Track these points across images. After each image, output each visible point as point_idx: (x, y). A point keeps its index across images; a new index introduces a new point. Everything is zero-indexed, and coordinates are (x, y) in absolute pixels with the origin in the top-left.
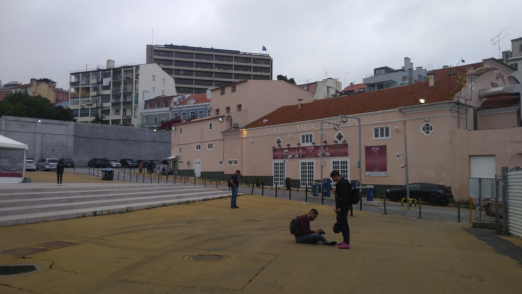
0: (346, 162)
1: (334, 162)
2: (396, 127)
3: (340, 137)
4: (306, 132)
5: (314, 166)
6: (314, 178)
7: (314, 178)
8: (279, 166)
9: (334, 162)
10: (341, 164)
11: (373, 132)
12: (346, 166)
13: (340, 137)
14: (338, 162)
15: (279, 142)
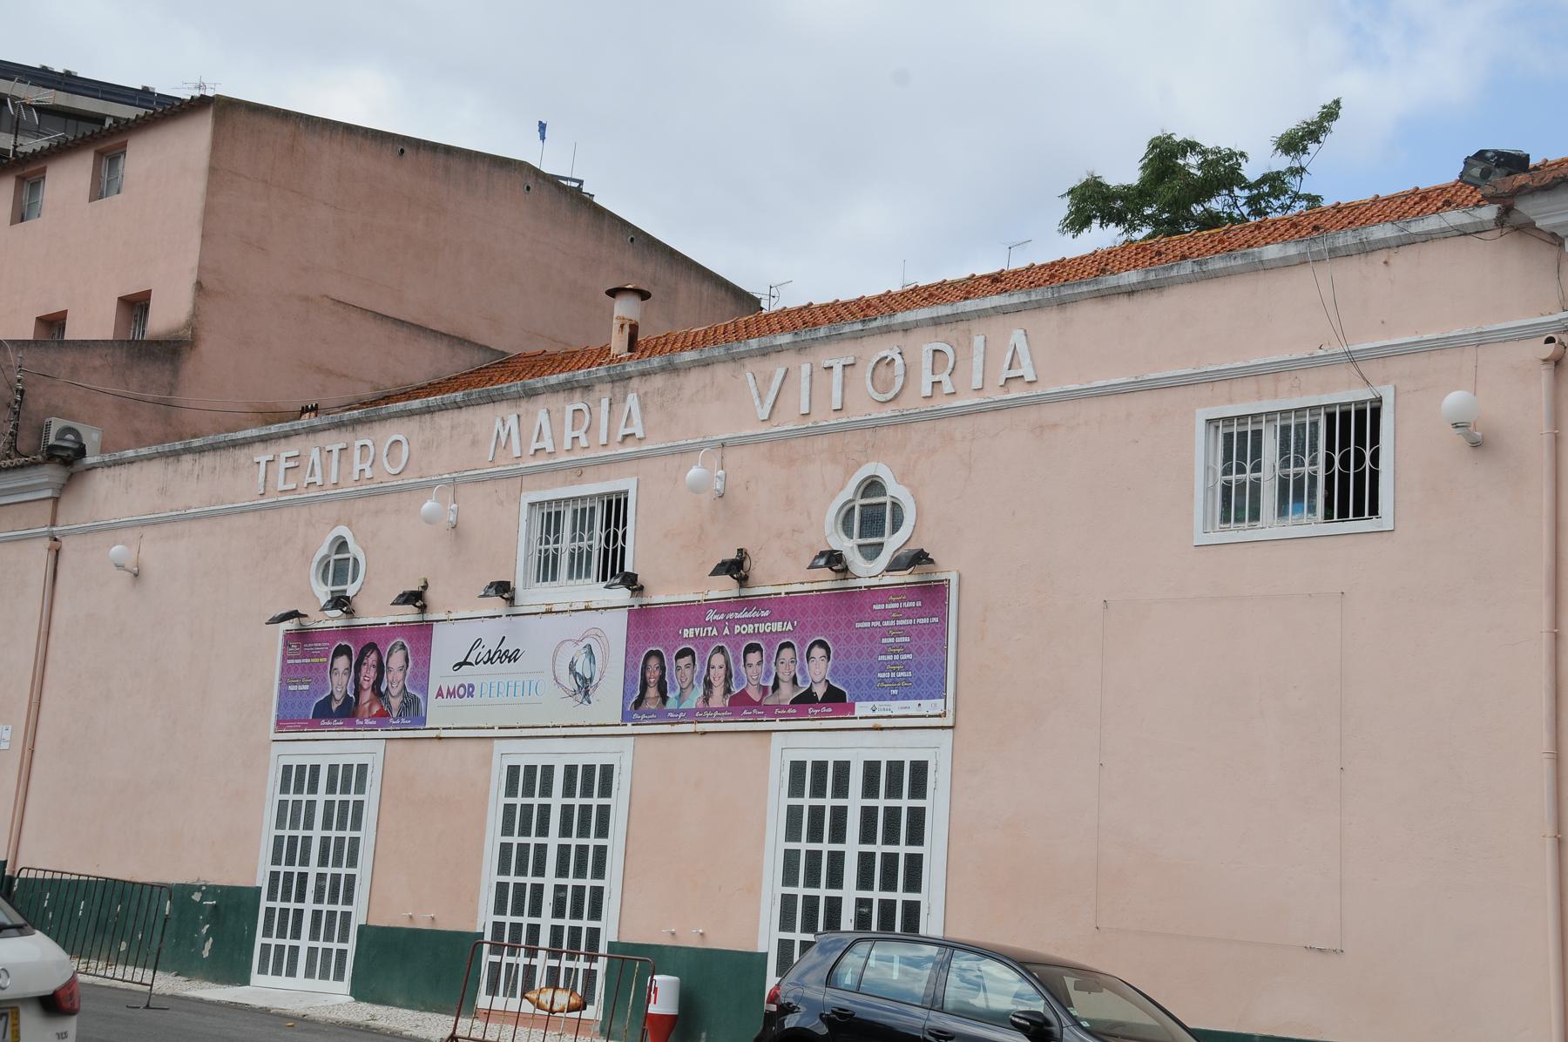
0: (920, 769)
1: (797, 768)
2: (1455, 400)
3: (872, 516)
4: (578, 470)
5: (936, 805)
6: (609, 930)
7: (609, 930)
8: (855, 802)
9: (513, 771)
10: (870, 789)
11: (1202, 461)
12: (917, 816)
13: (872, 516)
14: (842, 769)
15: (339, 567)
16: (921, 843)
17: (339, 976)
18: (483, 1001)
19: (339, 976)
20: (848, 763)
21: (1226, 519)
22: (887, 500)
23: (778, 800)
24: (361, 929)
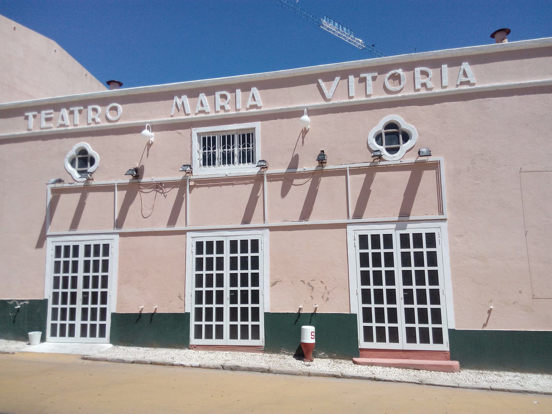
0: (106, 247)
1: (58, 249)
6: (112, 307)
14: (76, 248)
16: (258, 268)
17: (102, 334)
18: (193, 341)
19: (102, 334)
20: (230, 241)
21: (204, 164)
22: (383, 131)
23: (191, 257)
24: (266, 314)
